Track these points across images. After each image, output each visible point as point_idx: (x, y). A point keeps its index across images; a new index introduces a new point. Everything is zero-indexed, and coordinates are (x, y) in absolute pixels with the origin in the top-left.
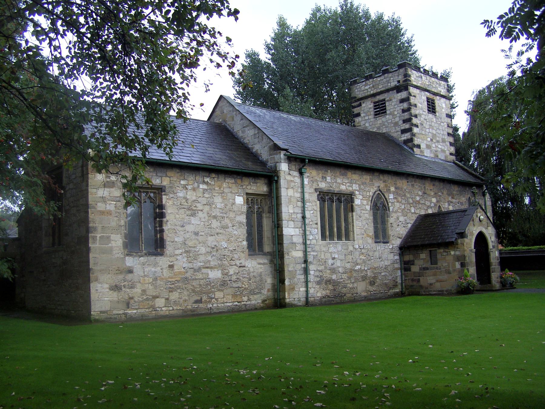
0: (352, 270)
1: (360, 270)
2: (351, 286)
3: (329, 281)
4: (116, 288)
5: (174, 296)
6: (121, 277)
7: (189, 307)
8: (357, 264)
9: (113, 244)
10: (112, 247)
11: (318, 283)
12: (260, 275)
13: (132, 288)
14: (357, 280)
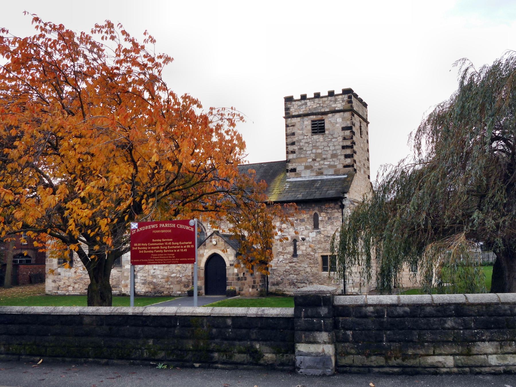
0: (168, 277)
1: (176, 277)
2: (168, 286)
3: (151, 283)
4: (54, 281)
5: (76, 286)
6: (56, 277)
7: (83, 292)
8: (173, 273)
9: (53, 263)
10: (53, 264)
11: (143, 284)
12: (119, 277)
13: (60, 281)
14: (172, 283)
